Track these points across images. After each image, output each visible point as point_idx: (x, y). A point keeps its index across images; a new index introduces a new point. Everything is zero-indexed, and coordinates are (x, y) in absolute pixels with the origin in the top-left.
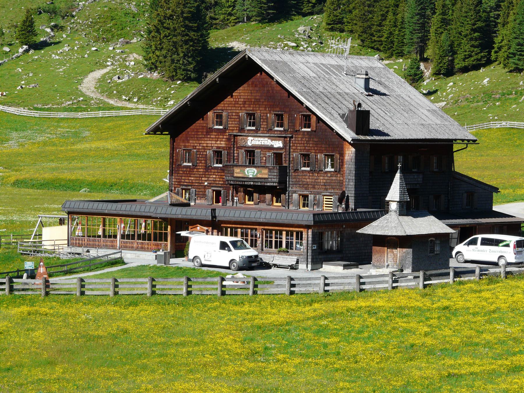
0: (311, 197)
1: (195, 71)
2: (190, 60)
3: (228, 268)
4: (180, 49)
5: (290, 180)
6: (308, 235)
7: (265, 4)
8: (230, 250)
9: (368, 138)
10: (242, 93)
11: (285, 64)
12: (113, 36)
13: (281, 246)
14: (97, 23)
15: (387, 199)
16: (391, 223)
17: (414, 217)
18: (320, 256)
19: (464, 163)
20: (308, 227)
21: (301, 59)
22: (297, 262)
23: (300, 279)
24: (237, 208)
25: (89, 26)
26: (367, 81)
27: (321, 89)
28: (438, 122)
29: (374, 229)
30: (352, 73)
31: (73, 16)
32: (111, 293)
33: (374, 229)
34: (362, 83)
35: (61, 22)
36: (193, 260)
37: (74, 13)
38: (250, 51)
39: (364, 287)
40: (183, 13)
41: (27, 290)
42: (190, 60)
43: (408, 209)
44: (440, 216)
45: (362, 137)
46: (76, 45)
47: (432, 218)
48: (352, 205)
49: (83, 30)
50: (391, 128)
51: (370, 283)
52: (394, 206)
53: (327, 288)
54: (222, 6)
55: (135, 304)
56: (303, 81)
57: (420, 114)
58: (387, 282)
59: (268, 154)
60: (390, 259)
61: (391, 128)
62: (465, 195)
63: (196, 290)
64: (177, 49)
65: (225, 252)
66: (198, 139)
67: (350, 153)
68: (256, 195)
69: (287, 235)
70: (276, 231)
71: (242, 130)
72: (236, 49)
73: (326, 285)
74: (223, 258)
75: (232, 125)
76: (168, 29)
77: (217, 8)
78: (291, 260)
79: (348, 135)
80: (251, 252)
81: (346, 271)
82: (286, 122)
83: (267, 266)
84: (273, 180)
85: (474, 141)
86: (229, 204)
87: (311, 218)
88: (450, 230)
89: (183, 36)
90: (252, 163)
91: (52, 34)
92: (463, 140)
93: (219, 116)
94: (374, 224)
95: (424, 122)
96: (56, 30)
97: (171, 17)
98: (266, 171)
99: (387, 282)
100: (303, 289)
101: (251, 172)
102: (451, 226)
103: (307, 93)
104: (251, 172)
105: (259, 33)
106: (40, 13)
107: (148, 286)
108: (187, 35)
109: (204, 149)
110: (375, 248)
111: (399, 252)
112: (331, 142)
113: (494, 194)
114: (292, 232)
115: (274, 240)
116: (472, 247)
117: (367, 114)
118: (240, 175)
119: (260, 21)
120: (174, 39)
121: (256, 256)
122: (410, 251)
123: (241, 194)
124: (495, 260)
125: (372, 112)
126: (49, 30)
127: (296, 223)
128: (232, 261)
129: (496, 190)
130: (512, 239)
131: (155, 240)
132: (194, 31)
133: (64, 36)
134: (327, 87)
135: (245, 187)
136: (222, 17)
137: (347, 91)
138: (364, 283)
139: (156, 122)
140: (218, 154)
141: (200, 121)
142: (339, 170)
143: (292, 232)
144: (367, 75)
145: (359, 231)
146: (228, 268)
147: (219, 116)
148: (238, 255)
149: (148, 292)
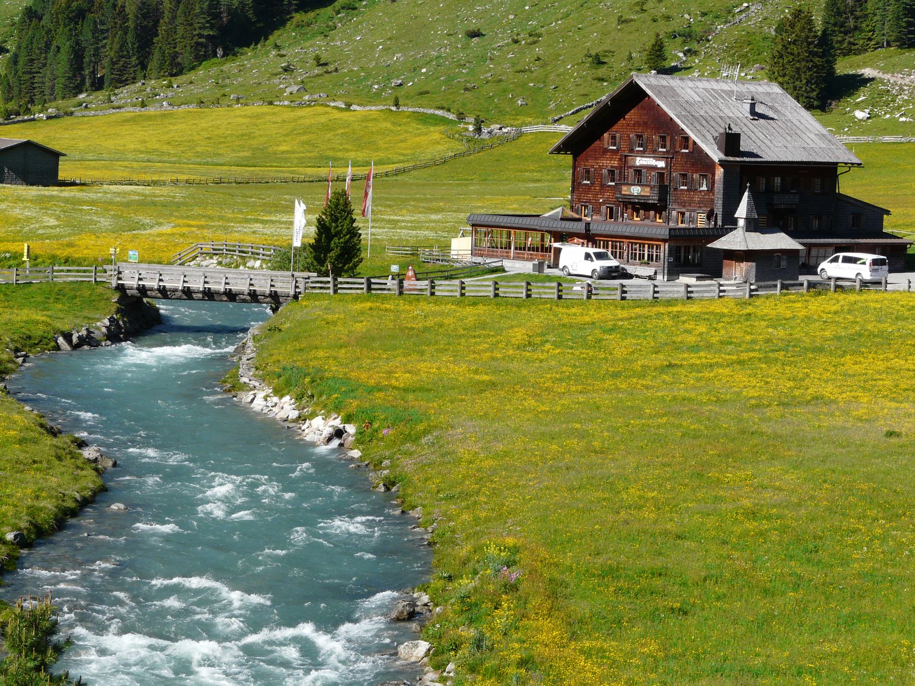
0: (687, 214)
1: (818, 98)
2: (813, 87)
3: (591, 277)
4: (803, 75)
5: (670, 198)
6: (665, 248)
7: (905, 28)
8: (592, 260)
9: (738, 159)
10: (632, 116)
11: (672, 88)
12: (748, 62)
13: (643, 258)
14: (732, 48)
15: (736, 216)
16: (737, 239)
17: (763, 233)
18: (676, 268)
19: (847, 186)
20: (665, 241)
21: (690, 84)
22: (656, 273)
23: (631, 286)
24: (627, 225)
25: (724, 51)
26: (753, 106)
27: (702, 113)
28: (823, 146)
29: (721, 244)
30: (740, 98)
31: (708, 41)
32: (458, 294)
33: (721, 244)
34: (747, 107)
35: (695, 46)
36: (563, 270)
37: (710, 37)
38: (637, 76)
39: (692, 295)
40: (808, 37)
41: (384, 289)
42: (813, 87)
43: (753, 226)
44: (793, 235)
45: (731, 159)
46: (707, 70)
47: (783, 235)
48: (720, 223)
49: (718, 55)
50: (767, 150)
51: (698, 292)
52: (741, 223)
53: (656, 295)
54: (862, 31)
55: (474, 304)
56: (686, 107)
57: (806, 138)
58: (714, 291)
59: (653, 173)
60: (738, 272)
61: (767, 150)
62: (851, 217)
63: (536, 293)
64: (800, 75)
65: (588, 262)
66: (596, 159)
67: (720, 172)
68: (642, 212)
69: (649, 248)
70: (640, 244)
71: (632, 151)
72: (866, 76)
73: (655, 292)
74: (586, 268)
75: (624, 146)
76: (792, 54)
77: (857, 33)
78: (650, 271)
79: (715, 154)
80: (613, 263)
81: (699, 283)
82: (668, 144)
83: (630, 277)
84: (654, 199)
85: (859, 164)
86: (620, 219)
87: (667, 232)
88: (800, 247)
89: (807, 62)
90: (639, 183)
91: (684, 59)
92: (846, 163)
93: (614, 138)
94: (723, 239)
95: (806, 146)
96: (689, 55)
97: (794, 42)
98: (648, 189)
99: (714, 291)
100: (635, 296)
101: (636, 190)
102: (801, 244)
103: (685, 117)
104: (636, 190)
105: (896, 59)
106: (675, 37)
107: (491, 289)
108: (812, 61)
109: (601, 168)
110: (725, 262)
111: (744, 265)
112: (706, 165)
113: (885, 216)
114: (653, 245)
115: (638, 252)
116: (834, 264)
117: (737, 137)
118: (627, 193)
119: (900, 47)
120: (798, 65)
121: (617, 267)
122: (754, 264)
123: (630, 211)
124: (853, 277)
125: (742, 134)
126: (681, 55)
127: (655, 236)
128: (594, 271)
129: (888, 212)
130: (869, 257)
131: (542, 251)
132: (819, 57)
133: (697, 61)
134: (709, 111)
135: (634, 204)
136: (861, 42)
137: (731, 115)
138: (692, 292)
139: (557, 142)
140: (612, 172)
141: (598, 142)
142: (711, 189)
143: (653, 245)
144: (753, 100)
145: (709, 246)
146: (591, 277)
147: (614, 138)
148: (599, 265)
149: (491, 294)
